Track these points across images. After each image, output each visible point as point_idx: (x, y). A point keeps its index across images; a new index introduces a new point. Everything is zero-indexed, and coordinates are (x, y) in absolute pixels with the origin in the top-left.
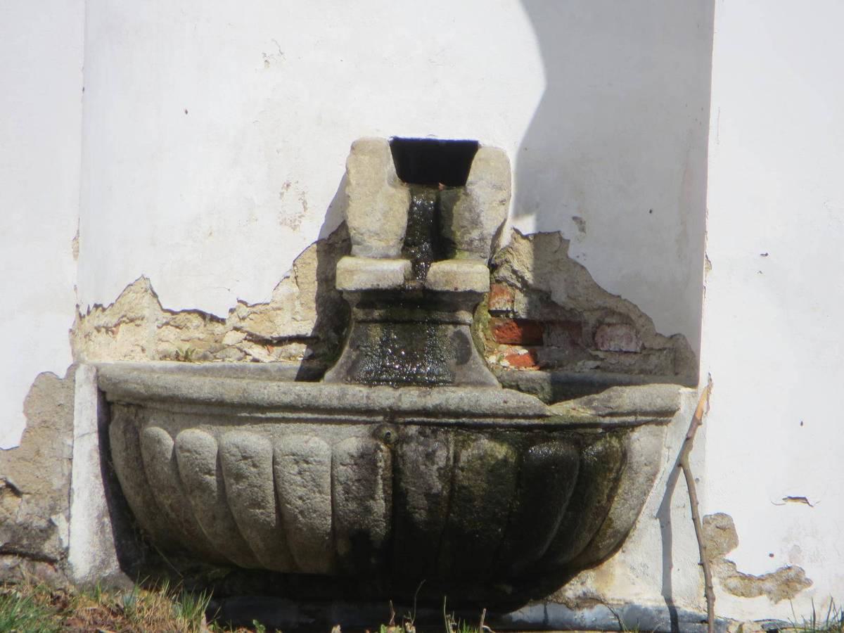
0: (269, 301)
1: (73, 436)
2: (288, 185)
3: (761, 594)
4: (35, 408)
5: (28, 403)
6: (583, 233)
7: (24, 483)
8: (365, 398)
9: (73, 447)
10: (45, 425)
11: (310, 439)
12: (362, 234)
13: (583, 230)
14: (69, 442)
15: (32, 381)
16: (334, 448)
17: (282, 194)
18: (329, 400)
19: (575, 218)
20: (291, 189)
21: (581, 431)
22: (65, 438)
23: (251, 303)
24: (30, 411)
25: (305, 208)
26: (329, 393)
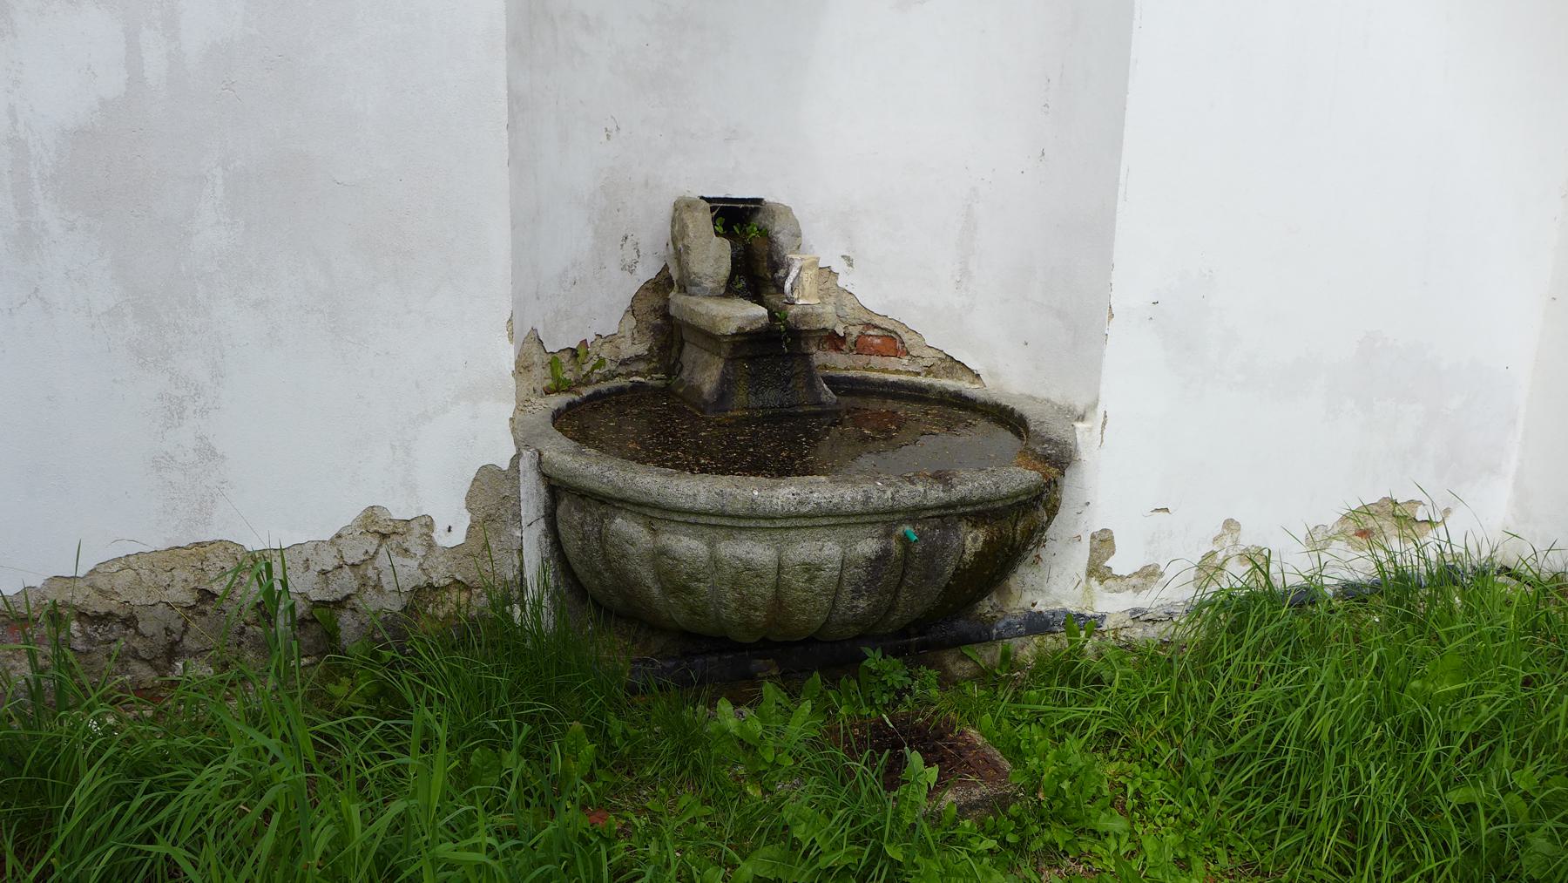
0: (616, 332)
1: (521, 527)
2: (626, 238)
3: (1127, 589)
4: (478, 502)
5: (470, 499)
6: (851, 268)
7: (473, 579)
8: (890, 500)
9: (522, 538)
10: (489, 518)
11: (823, 546)
12: (700, 278)
13: (851, 265)
14: (518, 534)
15: (473, 475)
16: (847, 551)
17: (622, 245)
18: (852, 506)
19: (843, 257)
20: (628, 240)
21: (675, 349)
22: (514, 530)
23: (604, 335)
24: (473, 506)
25: (639, 256)
26: (852, 498)
